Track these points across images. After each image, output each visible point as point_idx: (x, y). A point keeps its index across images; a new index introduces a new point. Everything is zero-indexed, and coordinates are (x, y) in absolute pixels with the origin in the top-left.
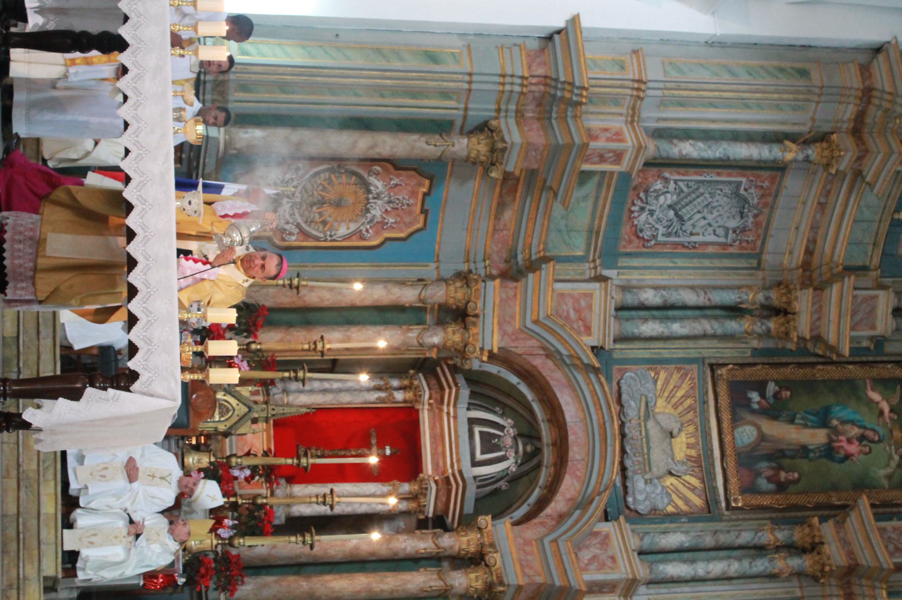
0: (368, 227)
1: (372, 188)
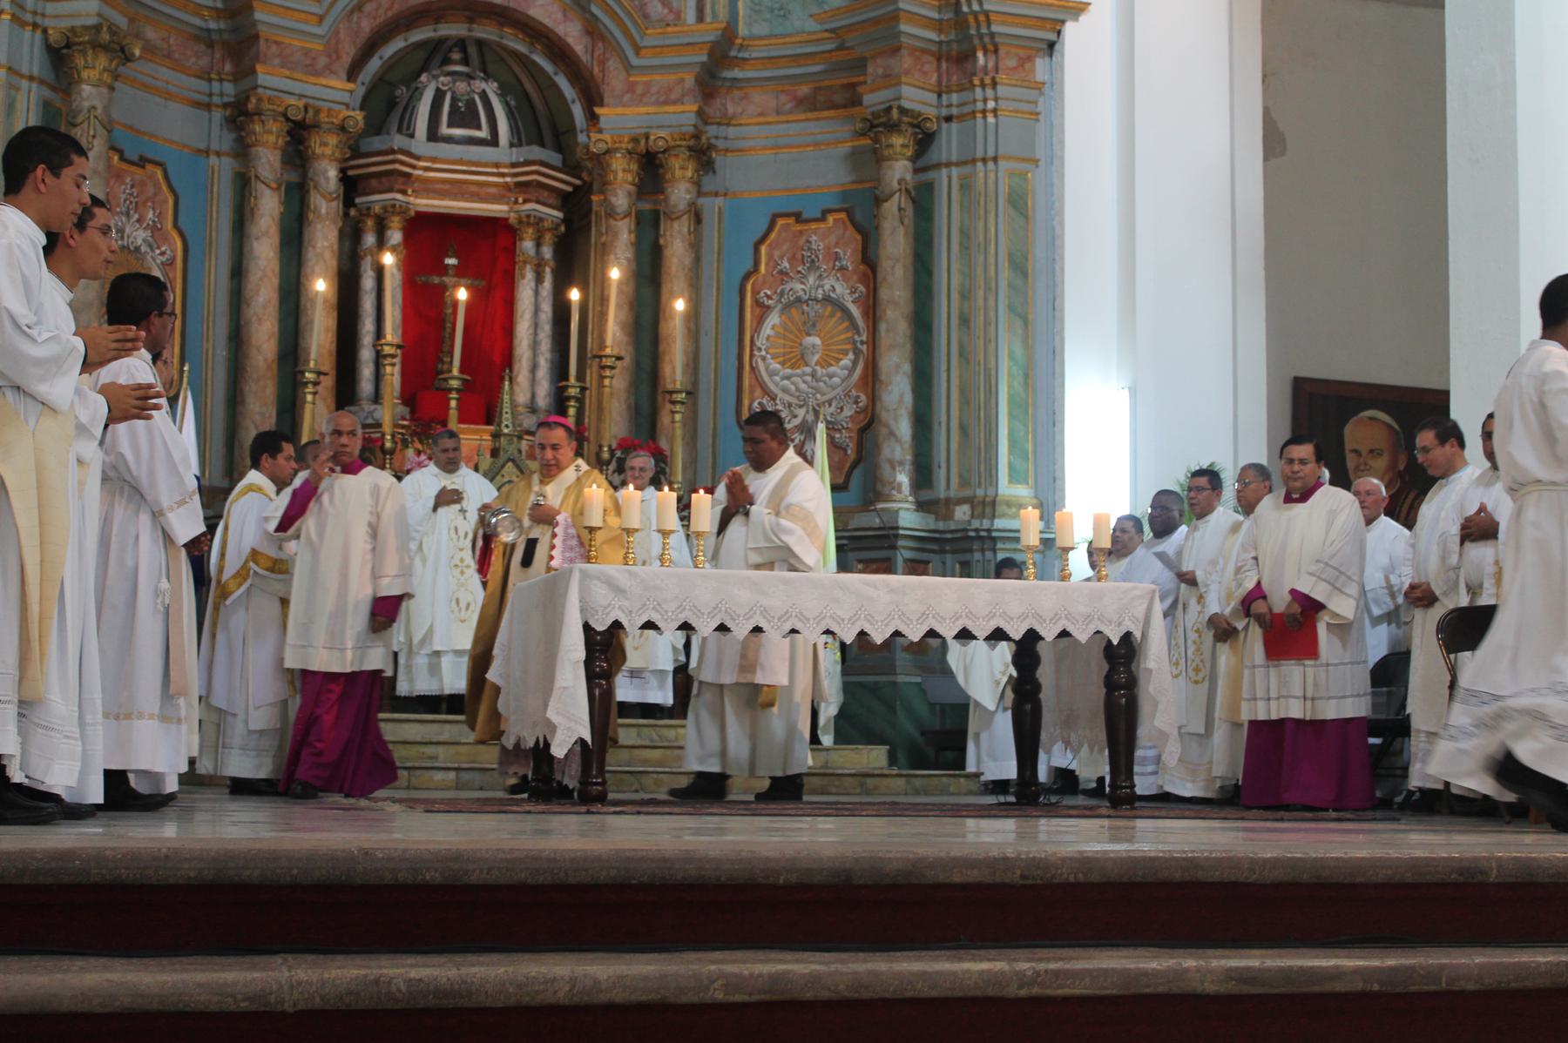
0: (158, 252)
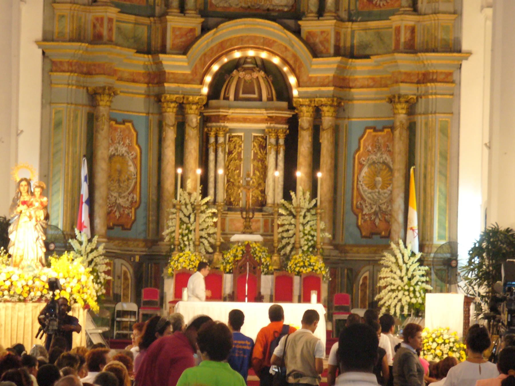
0: (130, 154)
1: (113, 153)
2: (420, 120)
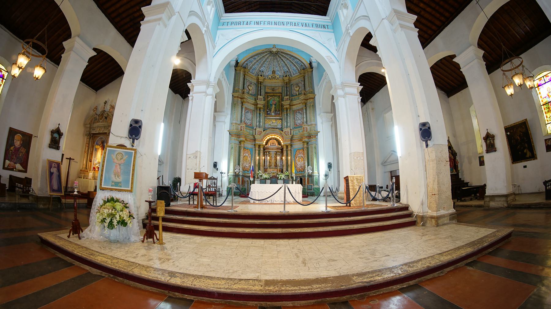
2: (309, 146)
